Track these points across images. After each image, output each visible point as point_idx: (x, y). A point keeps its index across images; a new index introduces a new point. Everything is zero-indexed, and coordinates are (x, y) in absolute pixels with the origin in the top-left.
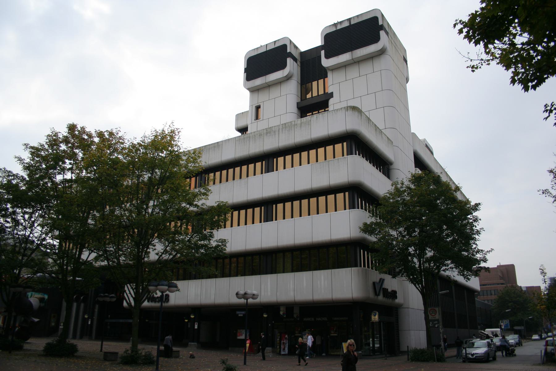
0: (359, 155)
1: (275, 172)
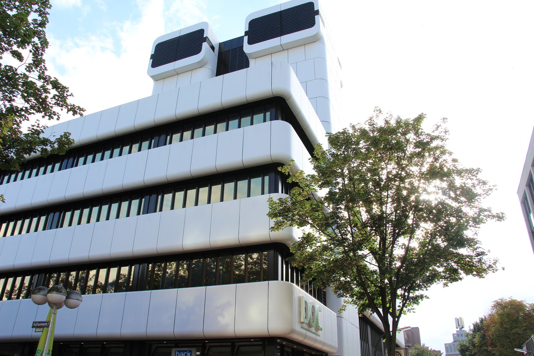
1: (158, 212)
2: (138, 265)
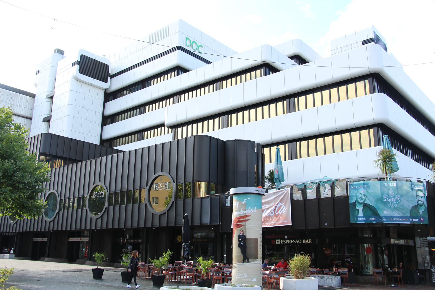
2: (223, 116)
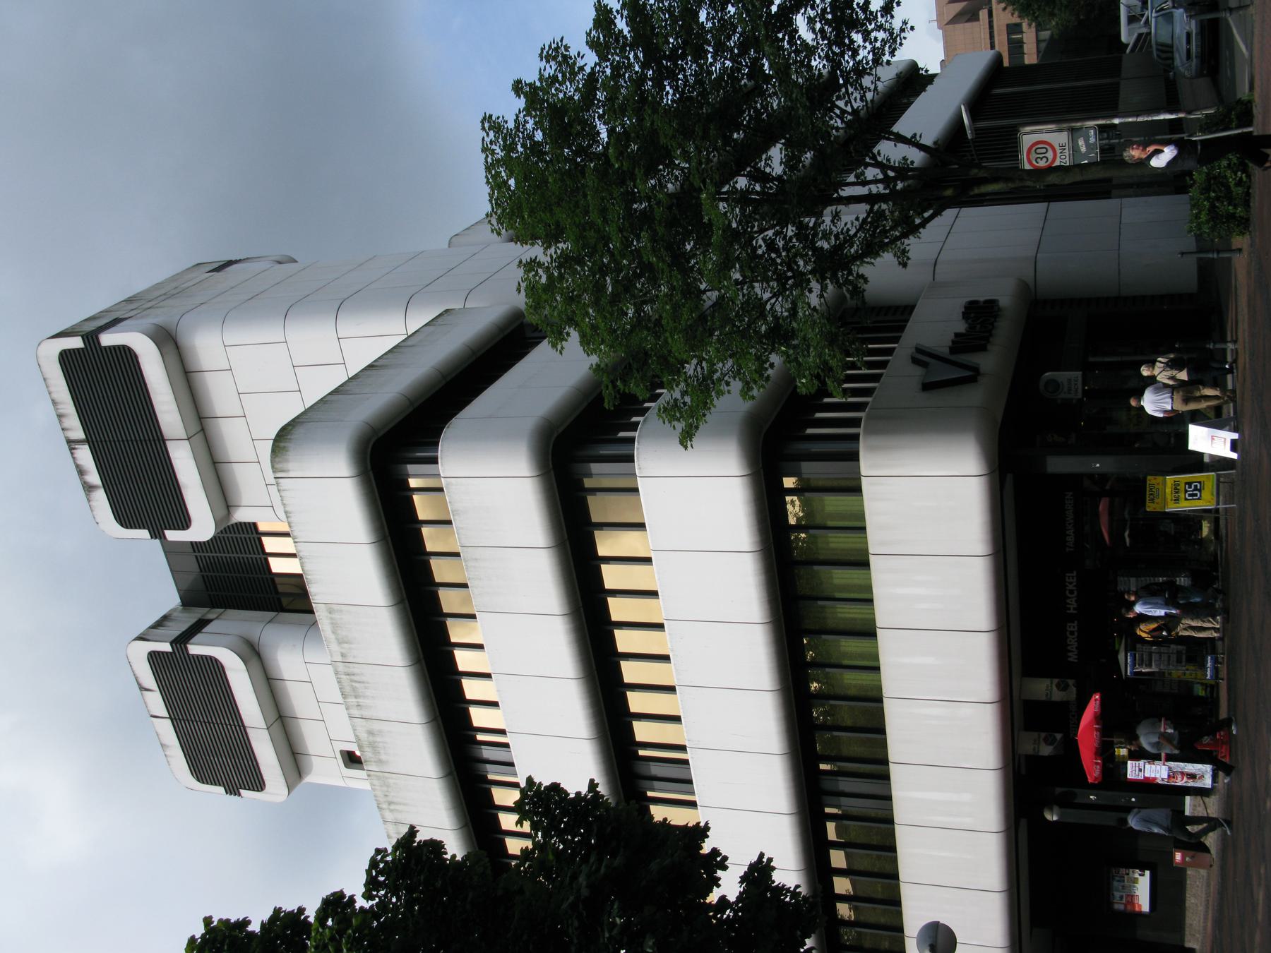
0: (634, 427)
